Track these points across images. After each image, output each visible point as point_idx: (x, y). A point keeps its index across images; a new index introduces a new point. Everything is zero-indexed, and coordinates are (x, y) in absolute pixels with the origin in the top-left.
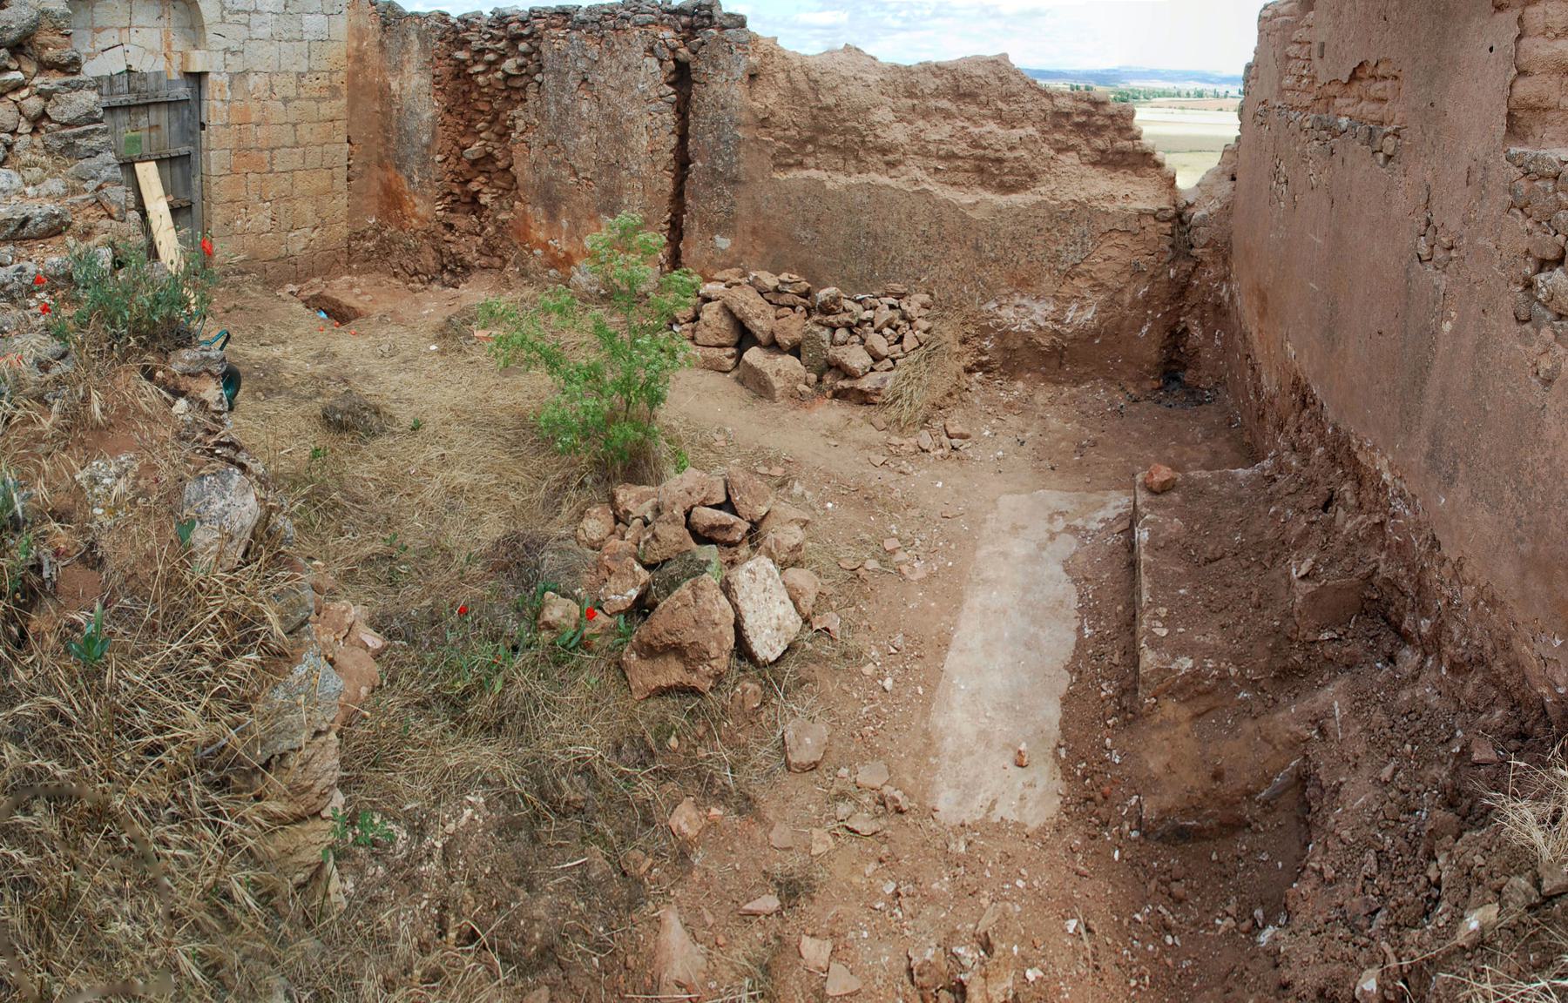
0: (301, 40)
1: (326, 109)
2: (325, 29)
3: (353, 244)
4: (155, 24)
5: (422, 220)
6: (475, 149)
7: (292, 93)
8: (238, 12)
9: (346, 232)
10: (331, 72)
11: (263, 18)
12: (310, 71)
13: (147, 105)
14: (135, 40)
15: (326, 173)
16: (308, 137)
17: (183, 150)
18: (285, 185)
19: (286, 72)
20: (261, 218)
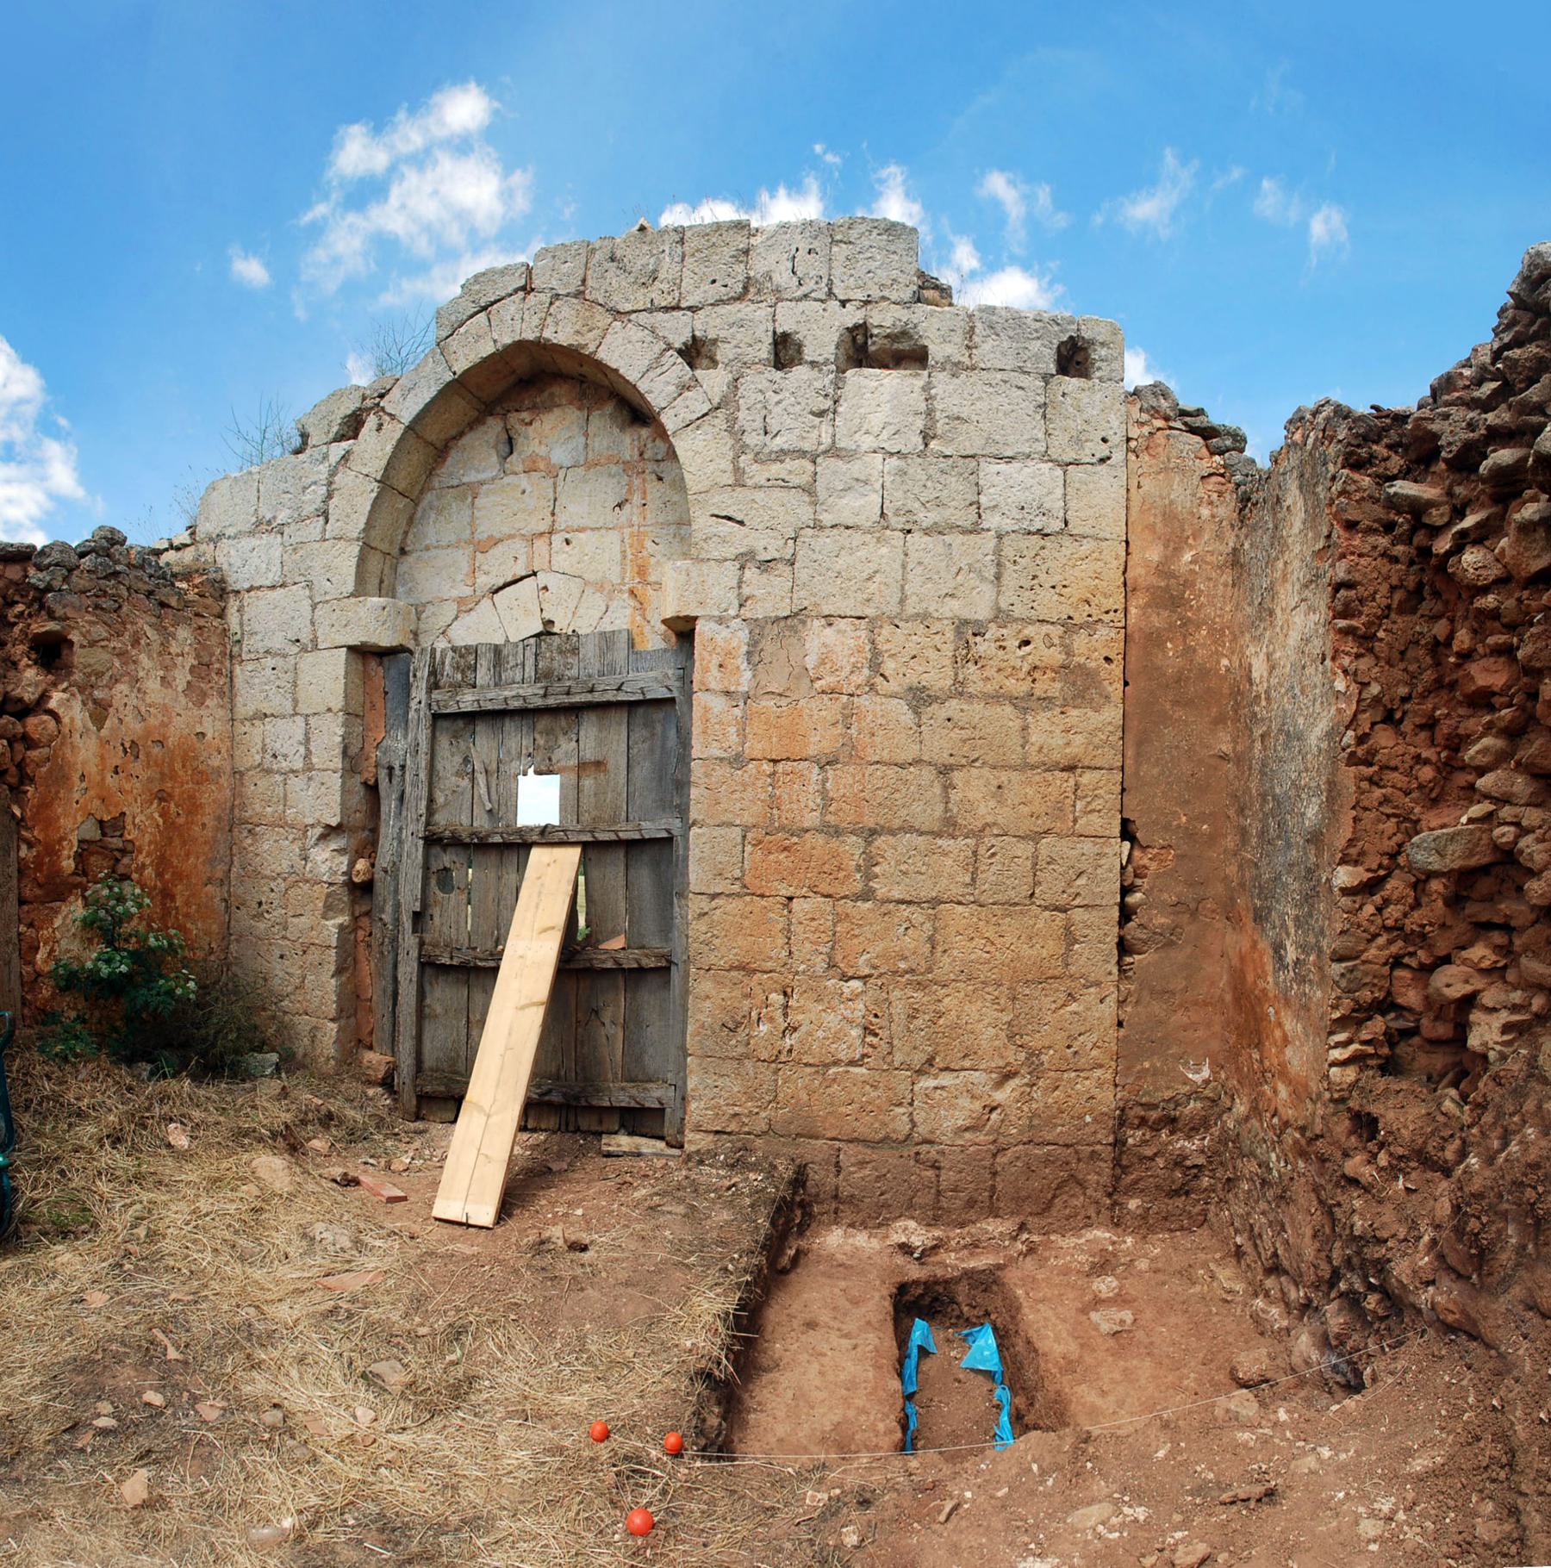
0: (975, 530)
1: (1049, 733)
3: (1133, 1137)
4: (611, 517)
5: (1300, 1093)
6: (1446, 837)
7: (938, 678)
8: (781, 455)
9: (1108, 1099)
11: (856, 468)
12: (1001, 617)
13: (575, 711)
15: (1044, 921)
16: (985, 810)
17: (652, 828)
18: (913, 942)
19: (924, 617)
20: (832, 1020)
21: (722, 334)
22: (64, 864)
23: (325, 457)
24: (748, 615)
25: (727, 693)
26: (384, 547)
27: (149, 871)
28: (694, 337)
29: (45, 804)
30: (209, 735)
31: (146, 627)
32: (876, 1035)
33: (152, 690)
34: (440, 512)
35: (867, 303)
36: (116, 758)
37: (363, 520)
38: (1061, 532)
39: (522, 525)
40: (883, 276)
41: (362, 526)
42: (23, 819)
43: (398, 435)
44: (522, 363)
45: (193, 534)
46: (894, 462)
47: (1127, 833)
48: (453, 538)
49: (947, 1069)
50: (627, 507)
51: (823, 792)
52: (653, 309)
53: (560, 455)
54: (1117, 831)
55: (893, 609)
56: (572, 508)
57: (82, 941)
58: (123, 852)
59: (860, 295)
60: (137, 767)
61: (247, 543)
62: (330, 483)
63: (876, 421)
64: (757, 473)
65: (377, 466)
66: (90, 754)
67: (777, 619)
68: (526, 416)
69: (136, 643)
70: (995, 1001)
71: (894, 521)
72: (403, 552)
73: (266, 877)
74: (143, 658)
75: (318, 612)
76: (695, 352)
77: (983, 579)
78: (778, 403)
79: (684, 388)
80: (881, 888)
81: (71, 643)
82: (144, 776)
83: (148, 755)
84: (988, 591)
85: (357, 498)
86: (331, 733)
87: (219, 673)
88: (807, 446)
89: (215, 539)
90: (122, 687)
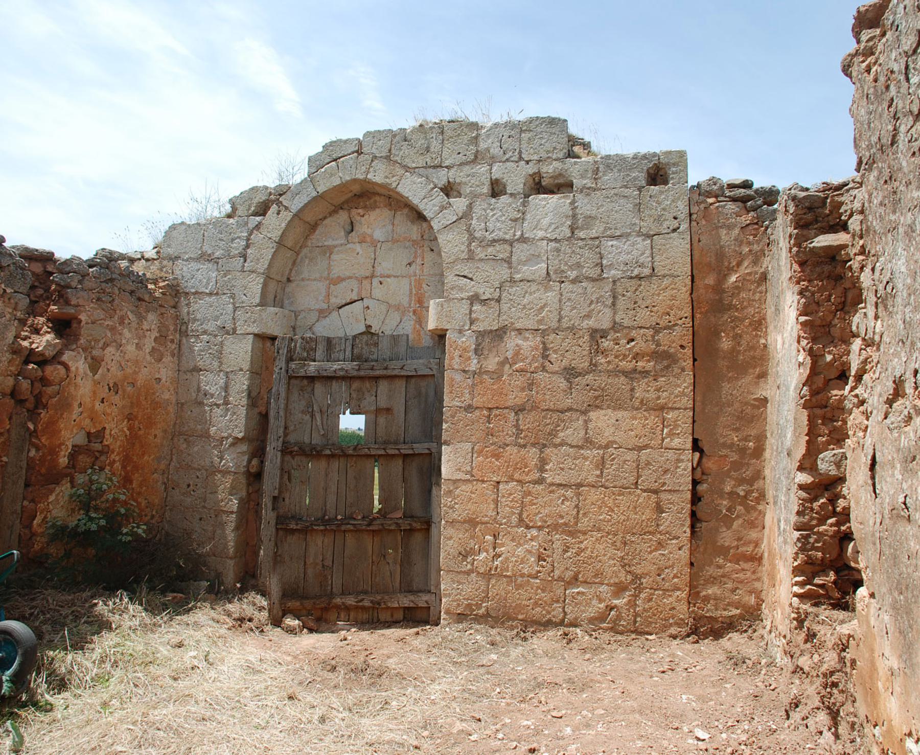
2: (646, 259)
10: (657, 329)
12: (616, 326)
14: (378, 292)
16: (608, 434)
17: (420, 448)
18: (567, 507)
19: (571, 329)
20: (520, 551)
21: (464, 180)
22: (61, 460)
23: (246, 223)
24: (476, 329)
25: (464, 371)
26: (279, 278)
27: (117, 465)
28: (449, 182)
29: (52, 423)
30: (164, 380)
31: (129, 313)
32: (545, 560)
33: (130, 349)
34: (311, 260)
35: (539, 161)
36: (104, 392)
37: (267, 263)
38: (651, 276)
39: (355, 271)
40: (548, 146)
41: (266, 266)
42: (35, 431)
43: (289, 219)
44: (356, 188)
45: (158, 252)
46: (553, 244)
47: (696, 446)
48: (318, 275)
49: (585, 582)
50: (414, 266)
51: (517, 426)
52: (427, 167)
53: (379, 234)
54: (689, 445)
55: (554, 324)
56: (384, 264)
57: (67, 510)
58: (101, 452)
59: (536, 157)
60: (116, 399)
61: (194, 265)
62: (248, 239)
63: (545, 222)
64: (480, 253)
65: (276, 235)
66: (87, 390)
67: (491, 331)
68: (361, 211)
69: (122, 322)
70: (614, 543)
71: (553, 277)
72: (289, 280)
73: (195, 469)
74: (126, 331)
75: (238, 313)
76: (449, 190)
77: (605, 306)
78: (494, 215)
79: (443, 208)
80: (549, 477)
81: (80, 321)
82: (120, 404)
83: (124, 391)
84: (608, 312)
85: (263, 253)
86: (241, 383)
87: (172, 341)
88: (507, 237)
89: (174, 259)
90: (110, 350)
